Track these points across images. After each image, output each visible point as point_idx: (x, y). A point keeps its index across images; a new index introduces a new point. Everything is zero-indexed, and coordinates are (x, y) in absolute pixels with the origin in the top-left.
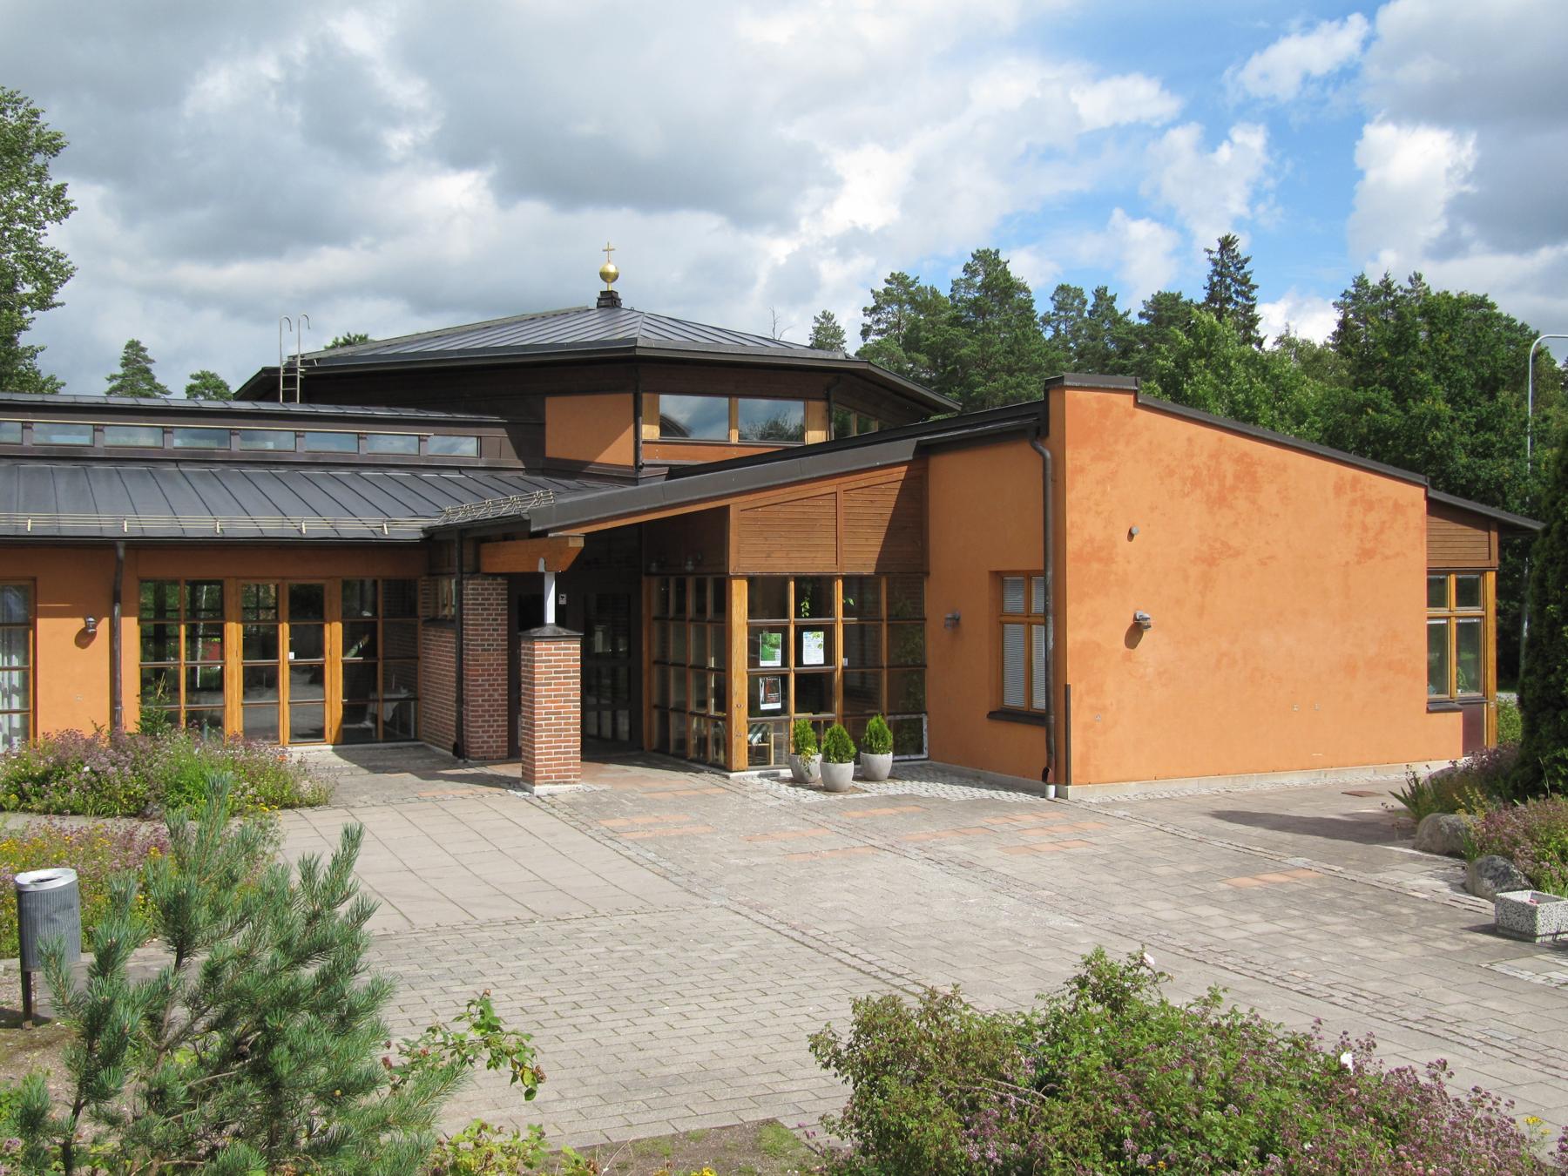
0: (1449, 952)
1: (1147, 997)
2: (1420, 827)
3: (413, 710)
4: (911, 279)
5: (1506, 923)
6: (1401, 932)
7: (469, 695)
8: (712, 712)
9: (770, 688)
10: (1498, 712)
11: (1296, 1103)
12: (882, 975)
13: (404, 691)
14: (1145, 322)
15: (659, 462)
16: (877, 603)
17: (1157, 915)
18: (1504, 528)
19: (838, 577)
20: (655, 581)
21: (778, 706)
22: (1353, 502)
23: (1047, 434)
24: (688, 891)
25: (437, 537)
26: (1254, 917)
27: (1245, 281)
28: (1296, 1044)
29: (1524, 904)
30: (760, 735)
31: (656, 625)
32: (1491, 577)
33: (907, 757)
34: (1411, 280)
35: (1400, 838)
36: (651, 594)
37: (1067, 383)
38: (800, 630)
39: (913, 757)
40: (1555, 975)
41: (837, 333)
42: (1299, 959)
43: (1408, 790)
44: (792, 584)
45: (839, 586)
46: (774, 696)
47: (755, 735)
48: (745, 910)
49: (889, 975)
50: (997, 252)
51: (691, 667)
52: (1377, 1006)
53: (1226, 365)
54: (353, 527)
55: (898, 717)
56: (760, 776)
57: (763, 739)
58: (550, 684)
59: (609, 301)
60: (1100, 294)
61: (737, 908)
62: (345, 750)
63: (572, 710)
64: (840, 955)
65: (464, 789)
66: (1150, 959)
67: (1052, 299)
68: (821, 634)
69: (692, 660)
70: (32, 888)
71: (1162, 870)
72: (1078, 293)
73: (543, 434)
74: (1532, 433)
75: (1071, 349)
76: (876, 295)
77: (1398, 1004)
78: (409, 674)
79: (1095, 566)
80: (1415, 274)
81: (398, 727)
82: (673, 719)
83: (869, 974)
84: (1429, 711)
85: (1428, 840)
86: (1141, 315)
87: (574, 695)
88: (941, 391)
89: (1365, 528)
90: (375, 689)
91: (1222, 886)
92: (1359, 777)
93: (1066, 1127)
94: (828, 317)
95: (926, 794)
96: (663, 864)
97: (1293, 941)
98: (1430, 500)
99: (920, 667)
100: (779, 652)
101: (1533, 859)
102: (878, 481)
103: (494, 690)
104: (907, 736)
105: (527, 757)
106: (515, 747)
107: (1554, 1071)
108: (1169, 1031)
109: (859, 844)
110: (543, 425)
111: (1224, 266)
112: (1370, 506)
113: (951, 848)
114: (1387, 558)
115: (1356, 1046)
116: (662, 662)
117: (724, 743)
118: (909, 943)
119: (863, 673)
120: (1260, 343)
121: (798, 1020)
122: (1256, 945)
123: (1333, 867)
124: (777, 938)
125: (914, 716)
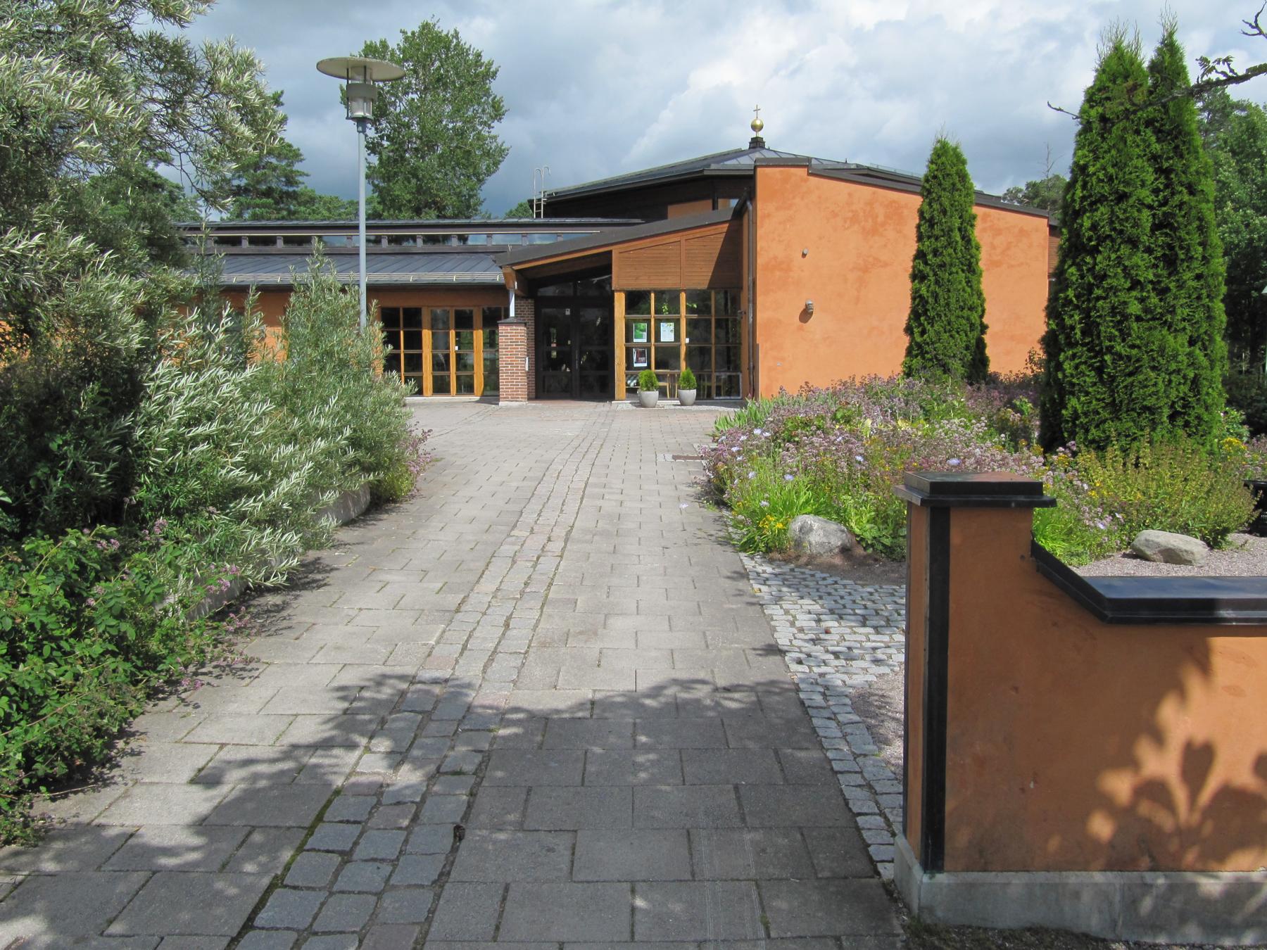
9: (641, 354)
21: (645, 365)
38: (658, 321)
46: (643, 359)
59: (757, 143)
68: (672, 324)
79: (778, 273)
100: (645, 334)
102: (708, 233)
114: (1012, 266)
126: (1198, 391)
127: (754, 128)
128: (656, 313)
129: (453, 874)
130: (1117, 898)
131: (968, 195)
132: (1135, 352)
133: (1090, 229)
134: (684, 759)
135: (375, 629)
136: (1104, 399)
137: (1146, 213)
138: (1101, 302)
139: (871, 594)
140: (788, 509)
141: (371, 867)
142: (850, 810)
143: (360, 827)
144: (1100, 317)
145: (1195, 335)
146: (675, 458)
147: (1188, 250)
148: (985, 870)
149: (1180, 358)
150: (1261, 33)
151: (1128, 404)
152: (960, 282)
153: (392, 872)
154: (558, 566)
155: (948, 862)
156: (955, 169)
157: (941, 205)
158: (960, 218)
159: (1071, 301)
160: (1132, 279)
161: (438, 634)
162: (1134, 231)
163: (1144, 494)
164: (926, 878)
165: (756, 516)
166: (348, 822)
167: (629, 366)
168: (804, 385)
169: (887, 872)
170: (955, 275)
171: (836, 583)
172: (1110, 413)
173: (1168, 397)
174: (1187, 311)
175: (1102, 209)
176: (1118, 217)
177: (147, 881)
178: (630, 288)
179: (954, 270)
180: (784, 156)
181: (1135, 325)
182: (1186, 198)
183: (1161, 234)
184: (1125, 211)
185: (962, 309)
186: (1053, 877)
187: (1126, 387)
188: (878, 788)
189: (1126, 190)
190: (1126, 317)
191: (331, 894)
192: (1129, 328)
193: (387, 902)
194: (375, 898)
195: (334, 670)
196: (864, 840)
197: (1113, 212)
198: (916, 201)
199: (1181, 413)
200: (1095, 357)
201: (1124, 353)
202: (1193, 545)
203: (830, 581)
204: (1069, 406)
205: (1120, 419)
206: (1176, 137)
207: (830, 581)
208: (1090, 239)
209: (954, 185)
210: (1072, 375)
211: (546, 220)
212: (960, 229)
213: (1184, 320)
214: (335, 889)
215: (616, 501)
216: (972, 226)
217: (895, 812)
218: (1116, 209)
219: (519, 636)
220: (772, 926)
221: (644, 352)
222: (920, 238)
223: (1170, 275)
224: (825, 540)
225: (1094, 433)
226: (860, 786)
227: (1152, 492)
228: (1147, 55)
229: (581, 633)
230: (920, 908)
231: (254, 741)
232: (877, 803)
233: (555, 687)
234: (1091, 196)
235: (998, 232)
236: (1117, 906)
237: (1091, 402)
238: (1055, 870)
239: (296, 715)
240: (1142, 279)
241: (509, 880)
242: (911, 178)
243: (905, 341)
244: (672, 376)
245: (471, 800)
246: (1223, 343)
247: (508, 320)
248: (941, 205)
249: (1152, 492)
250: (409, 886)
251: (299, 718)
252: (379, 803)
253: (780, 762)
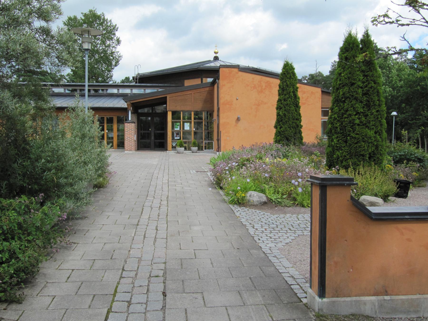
9: (177, 134)
19: (181, 111)
38: (184, 122)
46: (178, 136)
59: (216, 58)
68: (189, 123)
79: (228, 106)
98: (322, 91)
100: (179, 127)
102: (202, 91)
126: (378, 149)
127: (215, 53)
128: (183, 119)
129: (167, 307)
130: (377, 304)
131: (295, 80)
132: (357, 136)
133: (342, 95)
134: (231, 270)
135: (111, 231)
136: (347, 152)
137: (360, 90)
138: (346, 119)
139: (277, 217)
140: (245, 190)
141: (139, 305)
142: (288, 284)
143: (130, 294)
144: (346, 124)
145: (377, 130)
146: (197, 172)
147: (374, 102)
148: (338, 297)
149: (372, 138)
150: (405, 40)
151: (355, 153)
152: (293, 110)
153: (147, 306)
154: (168, 209)
155: (326, 296)
156: (291, 71)
157: (286, 83)
158: (293, 88)
159: (336, 119)
160: (356, 111)
161: (134, 232)
162: (357, 95)
163: (362, 183)
164: (320, 300)
165: (235, 192)
166: (126, 292)
168: (241, 146)
169: (305, 301)
170: (292, 108)
171: (264, 214)
172: (350, 156)
173: (368, 151)
174: (374, 122)
175: (346, 88)
176: (351, 91)
177: (66, 312)
178: (173, 110)
179: (291, 106)
180: (233, 64)
181: (357, 127)
182: (373, 85)
183: (366, 97)
184: (354, 89)
185: (294, 119)
186: (358, 298)
187: (354, 148)
188: (295, 277)
189: (354, 82)
190: (354, 124)
191: (129, 314)
192: (356, 128)
193: (148, 315)
194: (144, 314)
195: (102, 245)
196: (295, 292)
197: (349, 89)
198: (278, 82)
199: (373, 157)
200: (344, 138)
201: (354, 136)
202: (379, 200)
203: (262, 213)
204: (336, 154)
205: (353, 159)
206: (369, 65)
207: (262, 213)
208: (342, 98)
209: (291, 76)
210: (337, 144)
211: (140, 84)
212: (293, 92)
213: (373, 125)
214: (129, 312)
215: (181, 187)
216: (297, 91)
217: (302, 284)
218: (351, 88)
219: (162, 233)
220: (273, 317)
221: (178, 133)
222: (279, 95)
223: (368, 110)
224: (259, 200)
225: (344, 163)
226: (289, 277)
227: (364, 183)
228: (360, 37)
229: (183, 231)
230: (319, 310)
231: (83, 268)
232: (296, 281)
233: (181, 249)
234: (342, 83)
235: (304, 93)
236: (377, 307)
237: (343, 153)
238: (358, 296)
239: (94, 260)
240: (359, 112)
241: (186, 307)
242: (271, 72)
243: (274, 131)
244: (189, 142)
245: (165, 284)
246: (385, 133)
247: (128, 121)
248: (286, 83)
249: (364, 183)
250: (153, 311)
251: (96, 261)
252: (134, 287)
253: (262, 270)
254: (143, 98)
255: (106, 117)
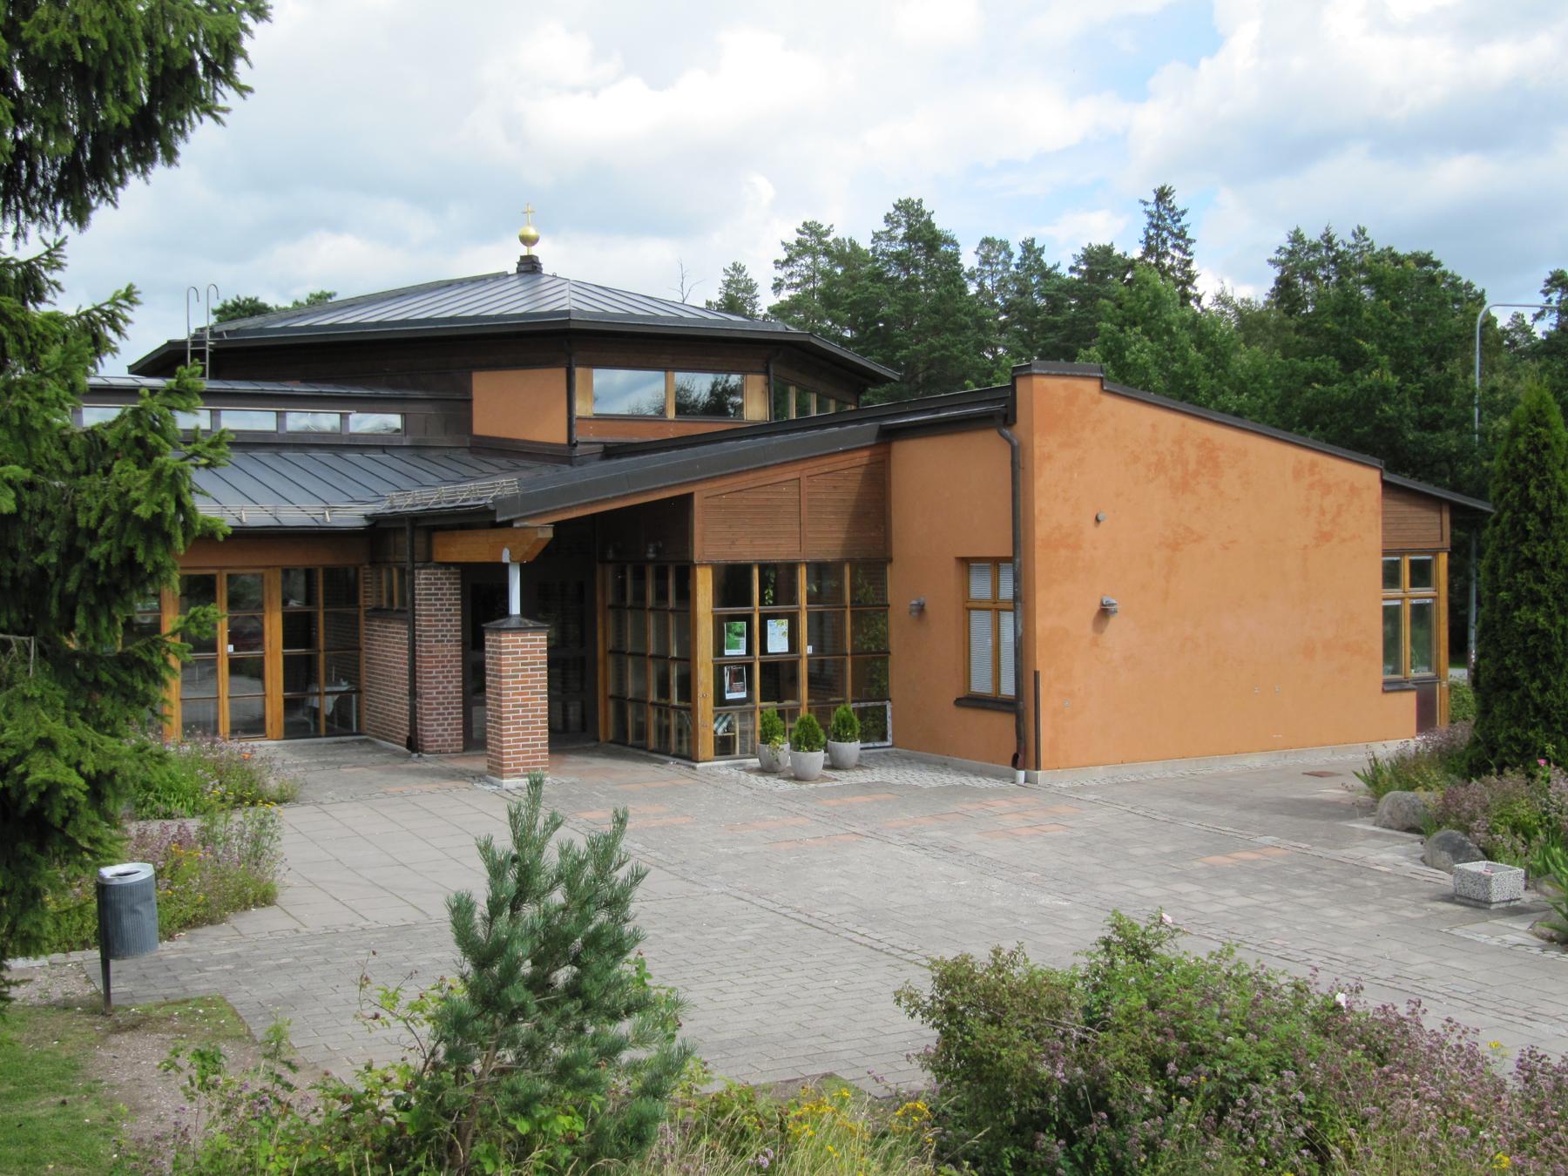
0: (1412, 919)
1: (1166, 951)
2: (1380, 805)
3: (354, 703)
4: (824, 229)
5: (1463, 892)
6: (1367, 903)
7: (424, 686)
8: (675, 702)
9: (736, 677)
10: (1450, 690)
11: (1308, 1037)
12: (893, 951)
13: (344, 683)
14: (1076, 276)
15: (593, 440)
16: (840, 589)
17: (1141, 892)
18: (1455, 508)
20: (610, 570)
21: (743, 695)
22: (1312, 486)
23: (1014, 421)
24: (683, 879)
25: (381, 525)
26: (1232, 892)
27: (1181, 235)
28: (1297, 987)
29: (1480, 874)
30: (725, 724)
31: (611, 615)
32: (1443, 559)
33: (871, 745)
34: (1354, 234)
35: (1362, 815)
36: (605, 580)
37: (1036, 371)
38: (764, 619)
39: (877, 744)
40: (1507, 937)
41: (750, 288)
42: (1277, 929)
43: (1367, 767)
44: (756, 572)
45: (802, 574)
46: (738, 684)
47: (720, 724)
48: (747, 896)
49: (901, 952)
50: (920, 201)
51: (651, 656)
52: (1351, 968)
53: (1169, 331)
54: (294, 515)
55: (863, 705)
56: (727, 766)
57: (729, 728)
58: (517, 676)
59: (529, 266)
60: (1028, 247)
61: (738, 894)
62: (288, 745)
63: (540, 703)
64: (849, 935)
65: (428, 785)
66: (1168, 919)
67: (977, 253)
68: (786, 622)
69: (652, 650)
70: (117, 882)
71: (1139, 851)
72: (1004, 246)
73: (470, 410)
74: (1478, 405)
75: (997, 304)
76: (787, 247)
77: (1369, 965)
78: (349, 665)
80: (1359, 228)
81: (336, 720)
82: (631, 711)
83: (881, 950)
84: (1384, 691)
85: (1388, 817)
86: (1072, 269)
87: (542, 687)
88: (864, 353)
89: (1323, 513)
90: (316, 681)
91: (1198, 864)
92: (1319, 758)
93: (1122, 1053)
94: (738, 269)
95: (896, 782)
96: (653, 854)
97: (1269, 913)
99: (884, 654)
100: (743, 640)
101: (1487, 831)
102: (841, 466)
103: (449, 682)
104: (871, 724)
105: (493, 751)
106: (474, 738)
107: (1509, 1018)
108: (1190, 979)
109: (840, 832)
110: (469, 401)
111: (1160, 217)
112: (1327, 489)
113: (933, 834)
114: (1343, 540)
115: (1347, 990)
116: (618, 653)
117: (688, 732)
118: (911, 922)
119: (822, 661)
120: (1199, 300)
121: (828, 992)
122: (1235, 917)
123: (1301, 845)
124: (784, 921)
125: (878, 704)
127: (527, 241)
167: (720, 700)
178: (722, 560)
221: (742, 671)
254: (585, 505)
255: (225, 573)
